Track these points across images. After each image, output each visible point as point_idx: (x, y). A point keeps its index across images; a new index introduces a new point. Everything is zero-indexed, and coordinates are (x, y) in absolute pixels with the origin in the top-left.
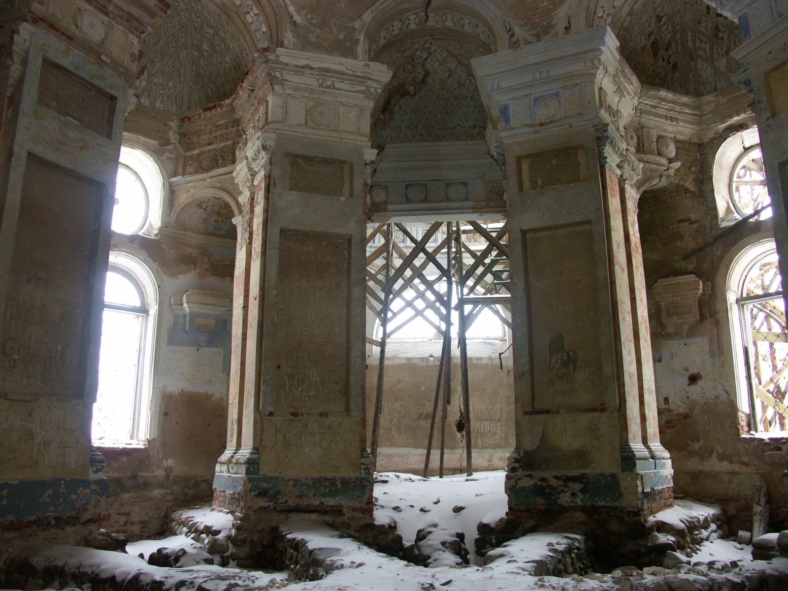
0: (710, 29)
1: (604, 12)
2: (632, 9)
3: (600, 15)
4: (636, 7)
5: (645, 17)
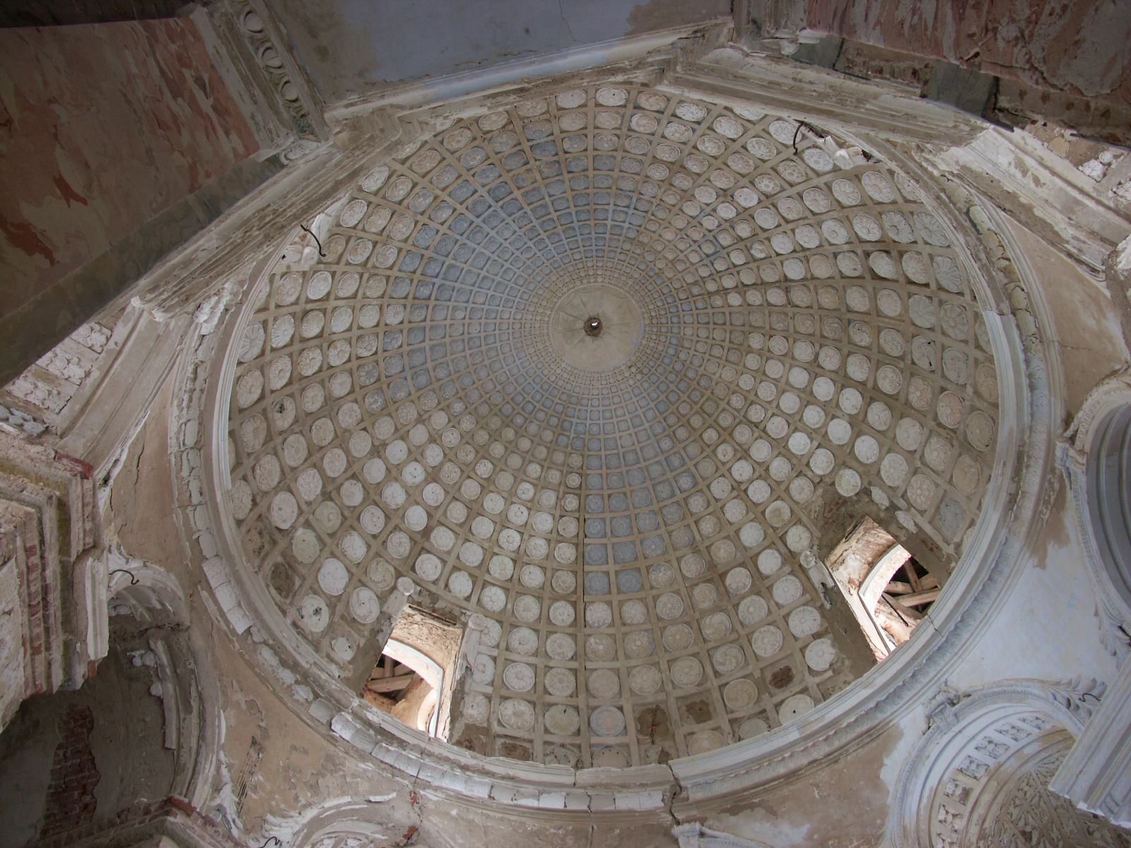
0: (1111, 841)
1: (943, 840)
2: (982, 830)
3: (941, 817)
4: (986, 825)
5: (1005, 838)
